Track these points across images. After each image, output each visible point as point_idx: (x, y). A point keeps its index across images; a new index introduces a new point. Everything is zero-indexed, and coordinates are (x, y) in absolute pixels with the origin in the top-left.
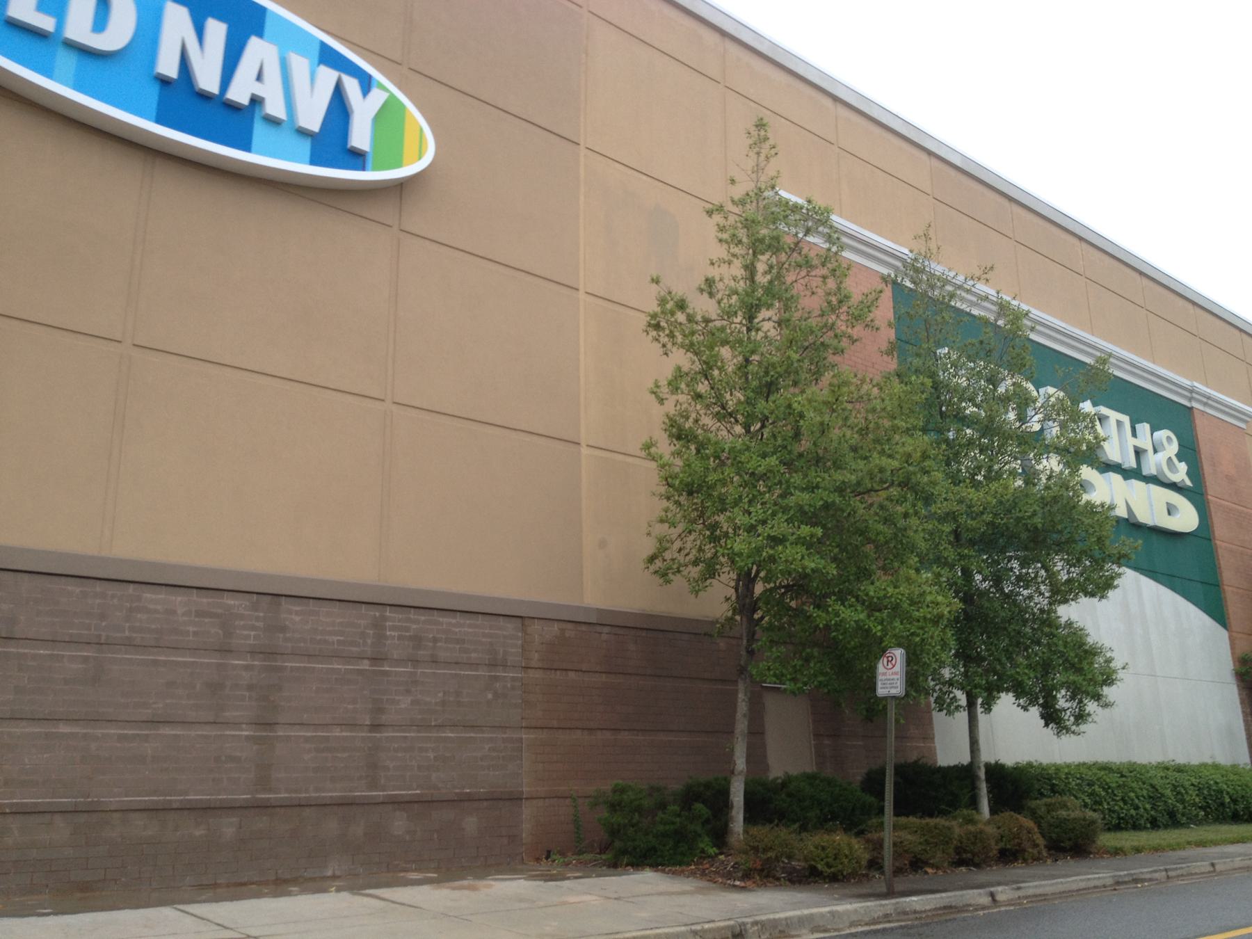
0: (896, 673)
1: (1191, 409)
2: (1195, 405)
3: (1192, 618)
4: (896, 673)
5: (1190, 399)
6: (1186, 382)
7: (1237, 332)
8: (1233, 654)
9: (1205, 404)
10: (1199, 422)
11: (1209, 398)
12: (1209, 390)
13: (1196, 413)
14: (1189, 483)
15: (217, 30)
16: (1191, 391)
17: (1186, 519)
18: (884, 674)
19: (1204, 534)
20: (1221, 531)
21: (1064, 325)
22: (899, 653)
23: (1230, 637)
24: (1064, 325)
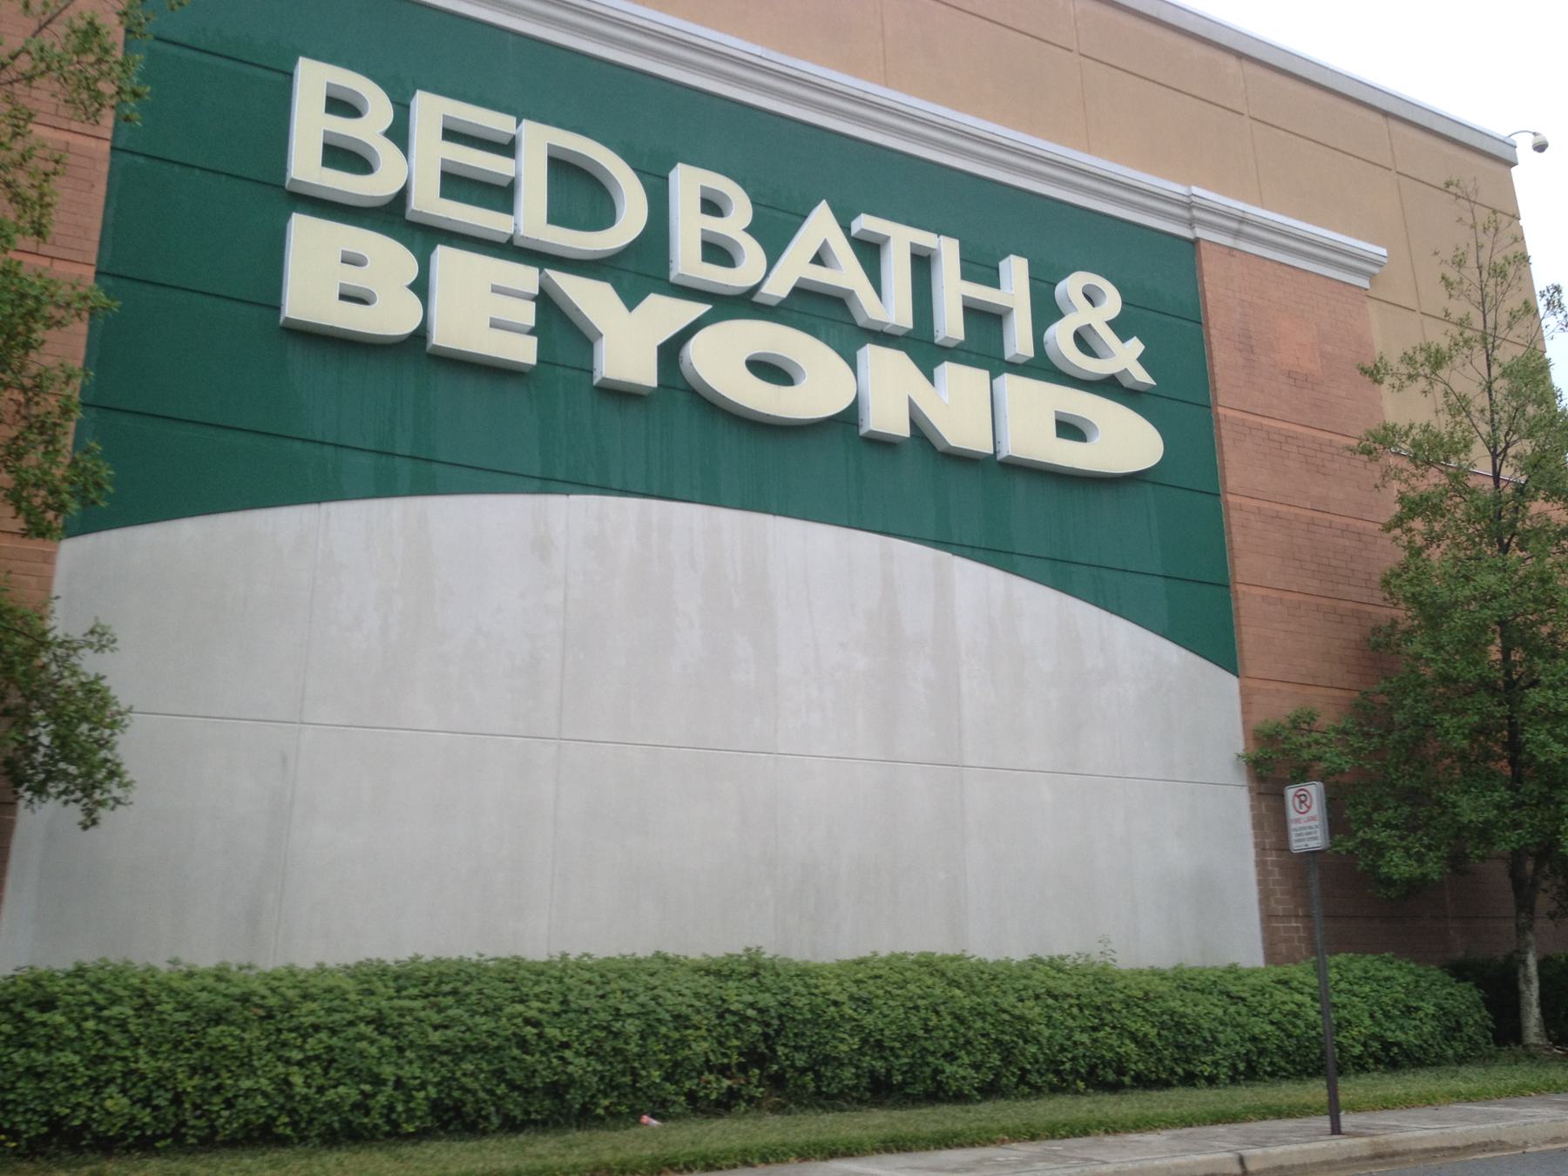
0: (1313, 819)
1: (1195, 242)
2: (1200, 233)
3: (1128, 656)
4: (1313, 819)
5: (1191, 223)
6: (1176, 189)
7: (1377, 119)
8: (1245, 723)
9: (1237, 234)
10: (1212, 272)
11: (1242, 221)
12: (1241, 206)
13: (1204, 251)
14: (1142, 376)
15: (1016, 270)
16: (1189, 206)
17: (1126, 443)
18: (1297, 821)
19: (1185, 486)
20: (1243, 473)
21: (758, 50)
22: (1314, 790)
23: (1243, 689)
24: (758, 50)
